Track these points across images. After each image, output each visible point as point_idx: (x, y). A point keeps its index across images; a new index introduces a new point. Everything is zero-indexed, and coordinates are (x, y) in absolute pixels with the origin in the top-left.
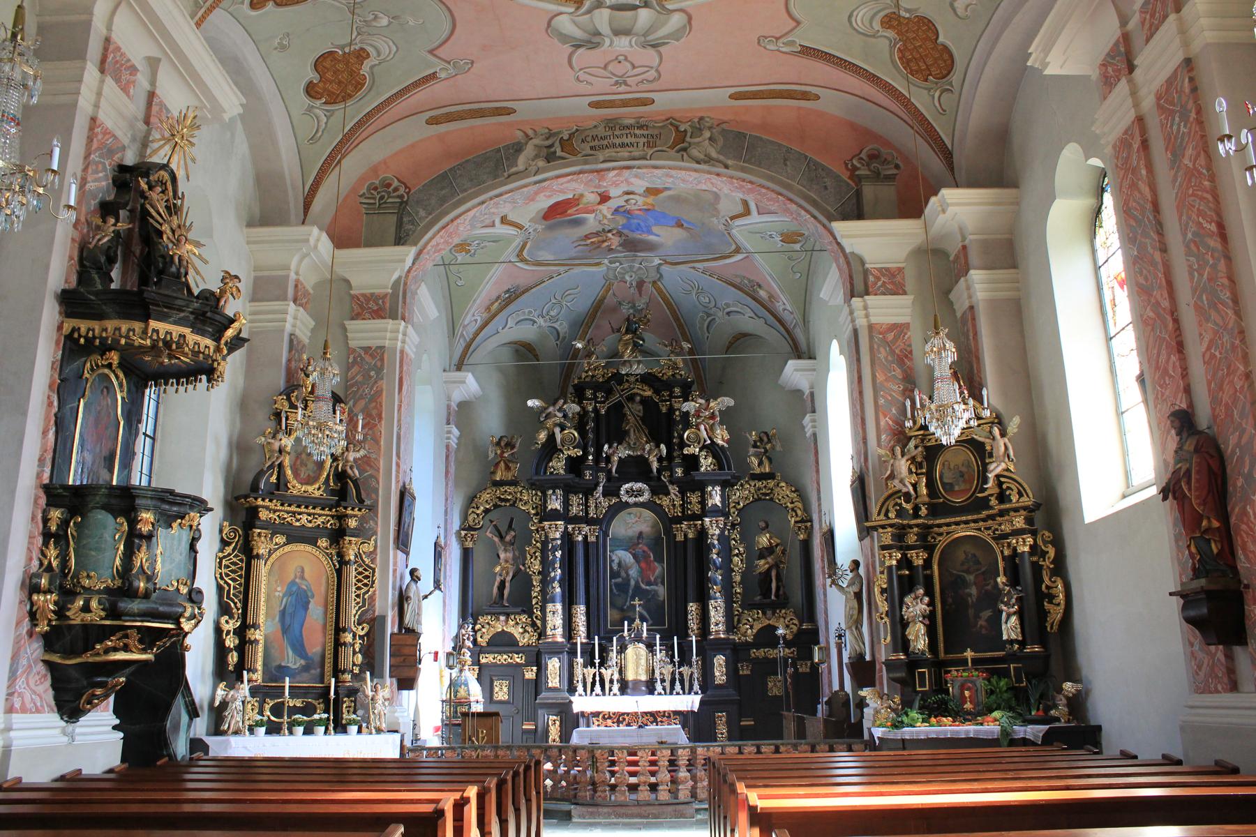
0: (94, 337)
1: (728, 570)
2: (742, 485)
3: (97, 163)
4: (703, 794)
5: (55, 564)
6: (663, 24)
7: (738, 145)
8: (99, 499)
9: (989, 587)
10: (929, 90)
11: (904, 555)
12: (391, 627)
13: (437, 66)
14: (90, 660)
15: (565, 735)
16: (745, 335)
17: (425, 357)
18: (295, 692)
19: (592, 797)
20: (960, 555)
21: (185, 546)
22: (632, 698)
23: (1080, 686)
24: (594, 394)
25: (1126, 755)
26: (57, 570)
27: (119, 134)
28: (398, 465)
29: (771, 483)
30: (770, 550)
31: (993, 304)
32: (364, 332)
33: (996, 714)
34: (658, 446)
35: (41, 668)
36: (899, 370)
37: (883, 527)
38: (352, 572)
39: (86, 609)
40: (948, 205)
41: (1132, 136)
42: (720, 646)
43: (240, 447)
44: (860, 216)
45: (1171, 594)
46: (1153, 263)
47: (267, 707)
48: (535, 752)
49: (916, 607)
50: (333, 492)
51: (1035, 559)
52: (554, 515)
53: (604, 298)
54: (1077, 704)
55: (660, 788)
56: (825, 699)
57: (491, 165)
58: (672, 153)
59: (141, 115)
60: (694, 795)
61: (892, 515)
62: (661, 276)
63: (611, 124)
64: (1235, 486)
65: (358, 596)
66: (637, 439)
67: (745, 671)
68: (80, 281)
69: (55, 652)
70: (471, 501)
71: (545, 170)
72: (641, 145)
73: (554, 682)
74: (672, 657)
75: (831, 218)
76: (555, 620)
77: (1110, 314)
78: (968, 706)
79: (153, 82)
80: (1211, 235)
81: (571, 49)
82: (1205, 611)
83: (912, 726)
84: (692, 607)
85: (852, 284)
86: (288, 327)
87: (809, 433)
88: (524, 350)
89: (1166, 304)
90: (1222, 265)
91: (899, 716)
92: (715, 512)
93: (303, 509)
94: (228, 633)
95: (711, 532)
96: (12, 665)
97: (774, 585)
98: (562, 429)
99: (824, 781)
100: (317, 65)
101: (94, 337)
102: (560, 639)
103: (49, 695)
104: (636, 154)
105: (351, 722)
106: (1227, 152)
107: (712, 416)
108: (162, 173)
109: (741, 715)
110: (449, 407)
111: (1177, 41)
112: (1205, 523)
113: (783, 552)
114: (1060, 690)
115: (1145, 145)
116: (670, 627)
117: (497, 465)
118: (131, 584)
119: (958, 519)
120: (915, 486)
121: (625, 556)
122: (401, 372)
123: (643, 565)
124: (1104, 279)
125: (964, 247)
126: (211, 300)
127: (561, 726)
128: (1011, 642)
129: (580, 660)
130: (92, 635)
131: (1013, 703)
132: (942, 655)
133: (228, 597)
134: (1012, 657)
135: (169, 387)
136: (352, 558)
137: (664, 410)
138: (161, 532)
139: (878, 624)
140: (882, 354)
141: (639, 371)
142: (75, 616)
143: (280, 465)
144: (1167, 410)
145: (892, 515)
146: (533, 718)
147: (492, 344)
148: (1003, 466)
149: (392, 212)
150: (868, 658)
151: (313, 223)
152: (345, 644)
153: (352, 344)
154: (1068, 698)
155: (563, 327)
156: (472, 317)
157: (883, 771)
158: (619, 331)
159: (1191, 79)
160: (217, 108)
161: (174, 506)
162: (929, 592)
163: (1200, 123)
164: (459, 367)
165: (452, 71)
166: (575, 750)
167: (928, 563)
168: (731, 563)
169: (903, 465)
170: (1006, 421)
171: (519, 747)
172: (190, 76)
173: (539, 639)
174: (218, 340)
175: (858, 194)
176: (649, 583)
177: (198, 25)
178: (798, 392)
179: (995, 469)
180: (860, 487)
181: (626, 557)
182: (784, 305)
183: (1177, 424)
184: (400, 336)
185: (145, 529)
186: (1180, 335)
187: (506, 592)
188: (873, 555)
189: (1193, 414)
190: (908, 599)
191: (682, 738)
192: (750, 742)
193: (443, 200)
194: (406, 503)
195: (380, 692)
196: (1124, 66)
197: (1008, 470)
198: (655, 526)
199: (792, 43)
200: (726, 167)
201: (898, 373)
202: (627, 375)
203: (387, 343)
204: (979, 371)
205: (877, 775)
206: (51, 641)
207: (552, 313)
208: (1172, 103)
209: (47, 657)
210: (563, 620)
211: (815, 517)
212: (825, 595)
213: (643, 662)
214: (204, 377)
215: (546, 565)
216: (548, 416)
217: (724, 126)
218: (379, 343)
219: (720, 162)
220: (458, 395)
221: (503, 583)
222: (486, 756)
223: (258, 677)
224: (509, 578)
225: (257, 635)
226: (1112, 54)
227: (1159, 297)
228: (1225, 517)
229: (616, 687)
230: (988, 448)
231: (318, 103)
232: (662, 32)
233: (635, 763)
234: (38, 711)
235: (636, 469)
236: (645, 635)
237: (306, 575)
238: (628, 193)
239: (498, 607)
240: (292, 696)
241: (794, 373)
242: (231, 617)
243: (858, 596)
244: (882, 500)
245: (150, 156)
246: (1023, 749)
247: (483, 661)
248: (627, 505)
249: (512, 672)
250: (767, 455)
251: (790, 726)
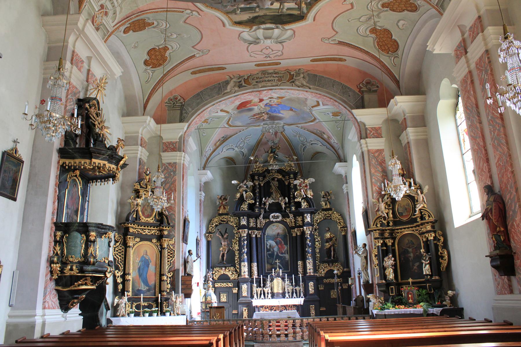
0: (71, 166)
1: (313, 247)
3: (70, 99)
4: (306, 338)
5: (59, 252)
6: (284, 35)
7: (314, 79)
8: (75, 227)
9: (418, 254)
10: (389, 57)
11: (384, 241)
12: (181, 273)
13: (195, 52)
14: (73, 289)
15: (250, 315)
16: (318, 153)
17: (191, 165)
18: (145, 300)
19: (262, 339)
20: (406, 241)
21: (107, 244)
22: (276, 300)
23: (454, 292)
24: (258, 178)
25: (471, 319)
26: (60, 255)
27: (78, 87)
28: (183, 209)
29: (330, 212)
30: (330, 239)
31: (417, 141)
32: (168, 157)
33: (422, 304)
34: (284, 198)
35: (54, 292)
36: (380, 168)
37: (375, 230)
38: (166, 252)
39: (71, 269)
40: (398, 102)
41: (467, 78)
42: (311, 278)
43: (121, 204)
44: (363, 107)
45: (486, 256)
46: (477, 128)
47: (134, 306)
48: (240, 322)
49: (389, 262)
50: (158, 221)
51: (435, 242)
52: (244, 227)
54: (454, 299)
55: (289, 335)
56: (354, 299)
57: (217, 89)
58: (288, 83)
59: (85, 79)
60: (302, 338)
61: (379, 225)
62: (284, 130)
63: (264, 72)
64: (509, 214)
65: (168, 261)
66: (276, 195)
67: (321, 288)
68: (65, 144)
69: (60, 286)
70: (210, 222)
71: (238, 91)
72: (276, 80)
73: (245, 294)
75: (352, 108)
76: (245, 269)
77: (463, 145)
78: (410, 301)
79: (89, 66)
80: (497, 118)
81: (248, 45)
82: (499, 263)
83: (388, 309)
84: (300, 263)
85: (361, 134)
86: (139, 156)
87: (345, 191)
88: (230, 161)
89: (482, 144)
90: (502, 129)
91: (383, 305)
92: (308, 224)
93: (146, 228)
94: (118, 277)
95: (307, 232)
96: (44, 291)
97: (332, 253)
98: (246, 192)
99: (353, 330)
100: (148, 53)
101: (71, 166)
102: (247, 277)
103: (57, 302)
104: (274, 84)
105: (167, 311)
106: (490, 103)
107: (306, 186)
108: (94, 101)
109: (320, 306)
110: (200, 184)
111: (483, 43)
112: (498, 229)
113: (336, 240)
114: (447, 294)
115: (472, 82)
116: (290, 271)
117: (220, 207)
118: (88, 260)
119: (405, 227)
120: (387, 214)
121: (272, 243)
122: (183, 172)
123: (280, 246)
124: (460, 131)
125: (405, 119)
126: (113, 149)
127: (248, 311)
128: (427, 275)
129: (255, 285)
130: (74, 279)
131: (428, 299)
132: (400, 281)
133: (118, 263)
134: (427, 281)
135: (98, 183)
136: (166, 246)
137: (287, 184)
138: (98, 239)
139: (374, 269)
140: (373, 161)
141: (276, 168)
142: (67, 272)
143: (137, 211)
144: (483, 185)
145: (379, 225)
146: (237, 309)
147: (217, 158)
148: (422, 205)
149: (178, 109)
150: (370, 282)
151: (148, 115)
152: (164, 280)
153: (164, 162)
154: (450, 297)
155: (245, 151)
156: (209, 148)
157: (378, 326)
158: (268, 152)
159: (488, 58)
160: (113, 74)
161: (102, 229)
162: (394, 256)
163: (492, 75)
164: (204, 168)
165: (201, 54)
166: (255, 321)
167: (393, 244)
168: (315, 245)
169: (382, 206)
170: (423, 187)
171: (233, 320)
172: (103, 63)
173: (238, 277)
174: (117, 165)
175: (362, 98)
176: (282, 253)
177: (105, 42)
178: (340, 176)
179: (419, 207)
180: (366, 214)
181: (273, 243)
182: (334, 140)
183: (487, 190)
184: (183, 158)
185: (92, 238)
186: (487, 156)
187: (225, 258)
188: (372, 242)
189: (493, 186)
190: (386, 259)
191: (297, 315)
192: (324, 317)
193: (198, 104)
194: (186, 224)
195: (178, 299)
196: (463, 51)
197: (424, 207)
198: (284, 230)
199: (335, 40)
200: (310, 88)
201: (380, 169)
202: (272, 170)
203: (177, 161)
204: (412, 168)
205: (375, 328)
206: (58, 282)
207: (241, 146)
208: (482, 67)
209: (57, 288)
210: (248, 269)
211: (348, 225)
212: (353, 257)
213: (280, 285)
214: (111, 179)
215: (241, 247)
216: (240, 187)
217: (308, 72)
218: (174, 161)
219: (308, 87)
220: (204, 179)
221: (223, 255)
222: (220, 324)
223: (130, 294)
224: (226, 252)
225: (130, 277)
226: (459, 46)
227: (479, 141)
228: (506, 227)
229: (270, 295)
230: (416, 198)
231: (149, 68)
232: (283, 38)
233: (279, 326)
234: (54, 308)
235: (276, 207)
236: (281, 274)
237: (148, 254)
238: (270, 98)
239: (222, 264)
240: (144, 301)
241: (339, 168)
242: (119, 270)
243: (366, 258)
244: (374, 219)
245: (90, 95)
246: (432, 317)
247: (216, 286)
248: (272, 222)
249: (228, 290)
250: (328, 201)
251: (340, 310)
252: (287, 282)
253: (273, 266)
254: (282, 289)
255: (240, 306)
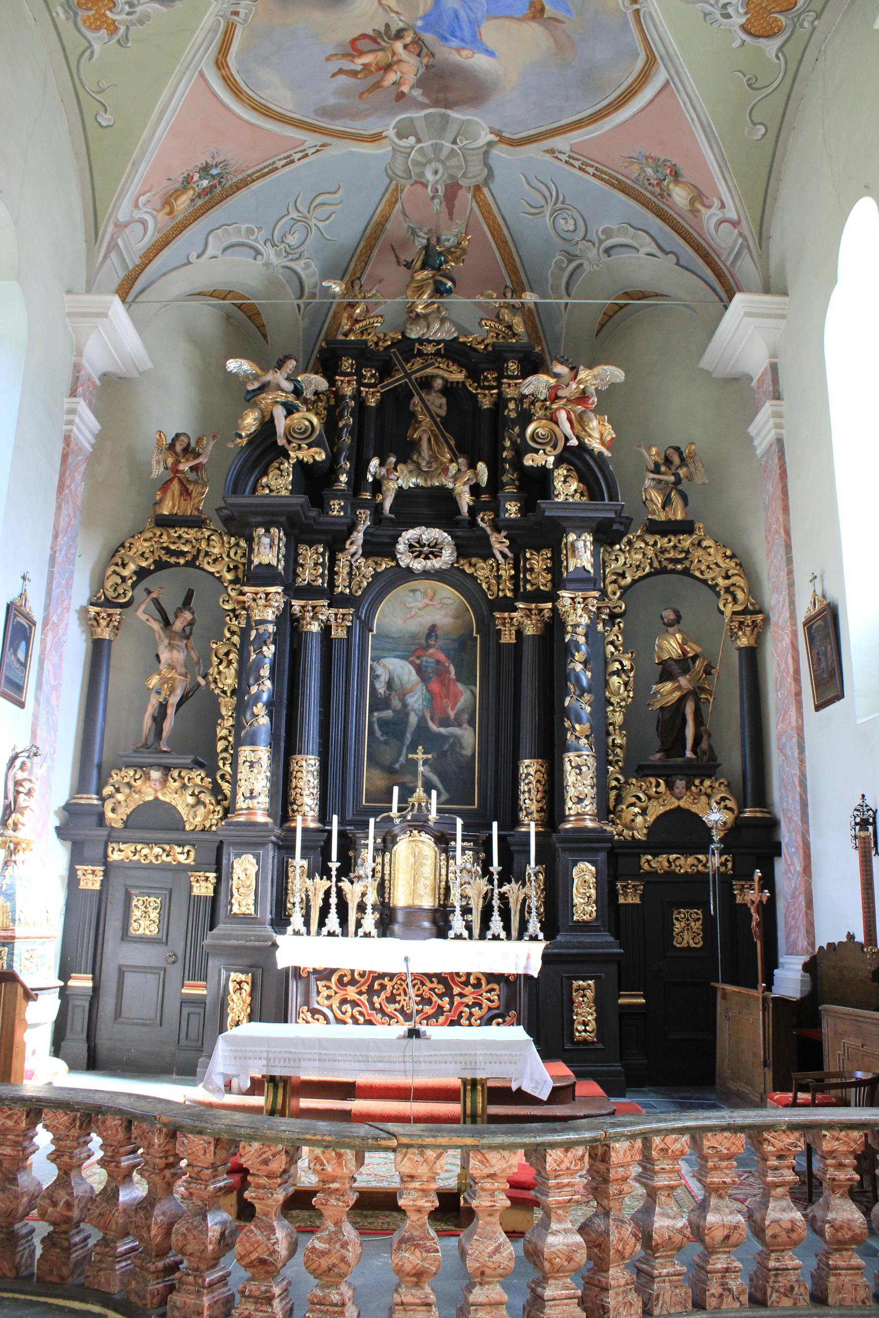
2: (630, 543)
29: (687, 542)
30: (684, 663)
34: (472, 466)
42: (585, 844)
52: (264, 576)
53: (381, 225)
67: (630, 898)
70: (115, 554)
73: (243, 902)
74: (488, 862)
76: (255, 779)
84: (530, 769)
95: (571, 620)
97: (690, 732)
109: (624, 984)
113: (708, 671)
116: (483, 808)
121: (398, 669)
123: (435, 686)
129: (299, 863)
137: (486, 404)
147: (178, 284)
173: (225, 816)
176: (445, 722)
187: (168, 725)
198: (459, 615)
202: (420, 341)
207: (293, 240)
210: (273, 780)
213: (428, 870)
215: (246, 673)
220: (97, 359)
221: (163, 707)
224: (174, 700)
229: (370, 921)
235: (435, 506)
236: (433, 815)
239: (150, 755)
247: (115, 856)
248: (409, 574)
250: (675, 489)
252: (463, 859)
253: (399, 774)
254: (436, 888)
255: (213, 963)
